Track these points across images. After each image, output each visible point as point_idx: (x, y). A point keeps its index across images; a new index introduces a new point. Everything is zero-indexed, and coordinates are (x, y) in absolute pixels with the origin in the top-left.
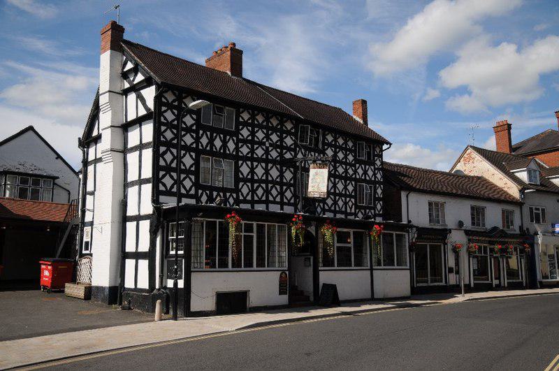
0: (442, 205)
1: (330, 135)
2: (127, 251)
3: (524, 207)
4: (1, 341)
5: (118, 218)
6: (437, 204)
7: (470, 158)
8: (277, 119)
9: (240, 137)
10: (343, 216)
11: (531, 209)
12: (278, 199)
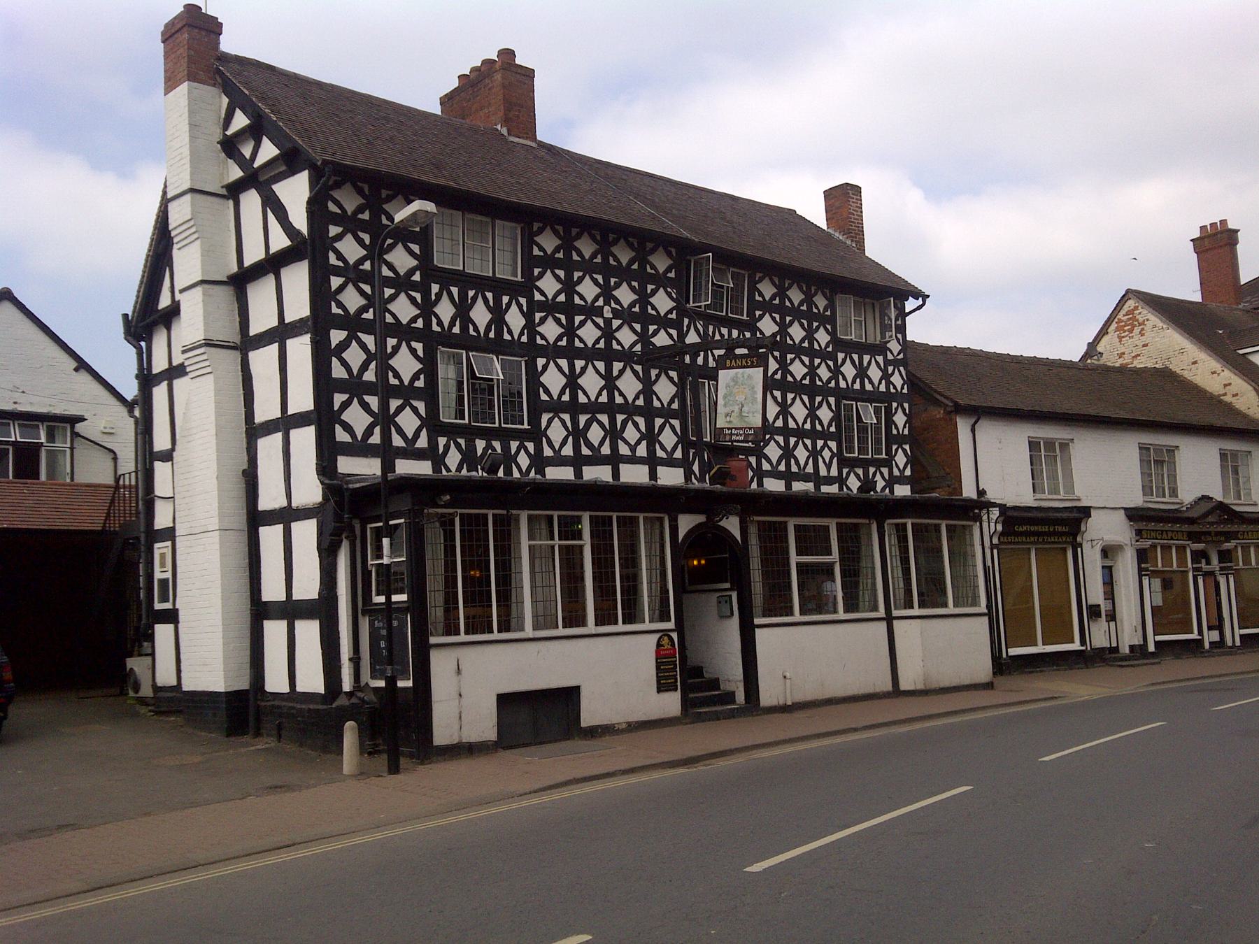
0: (1065, 446)
1: (548, 231)
6: (1050, 444)
9: (538, 297)
10: (810, 486)
12: (642, 451)
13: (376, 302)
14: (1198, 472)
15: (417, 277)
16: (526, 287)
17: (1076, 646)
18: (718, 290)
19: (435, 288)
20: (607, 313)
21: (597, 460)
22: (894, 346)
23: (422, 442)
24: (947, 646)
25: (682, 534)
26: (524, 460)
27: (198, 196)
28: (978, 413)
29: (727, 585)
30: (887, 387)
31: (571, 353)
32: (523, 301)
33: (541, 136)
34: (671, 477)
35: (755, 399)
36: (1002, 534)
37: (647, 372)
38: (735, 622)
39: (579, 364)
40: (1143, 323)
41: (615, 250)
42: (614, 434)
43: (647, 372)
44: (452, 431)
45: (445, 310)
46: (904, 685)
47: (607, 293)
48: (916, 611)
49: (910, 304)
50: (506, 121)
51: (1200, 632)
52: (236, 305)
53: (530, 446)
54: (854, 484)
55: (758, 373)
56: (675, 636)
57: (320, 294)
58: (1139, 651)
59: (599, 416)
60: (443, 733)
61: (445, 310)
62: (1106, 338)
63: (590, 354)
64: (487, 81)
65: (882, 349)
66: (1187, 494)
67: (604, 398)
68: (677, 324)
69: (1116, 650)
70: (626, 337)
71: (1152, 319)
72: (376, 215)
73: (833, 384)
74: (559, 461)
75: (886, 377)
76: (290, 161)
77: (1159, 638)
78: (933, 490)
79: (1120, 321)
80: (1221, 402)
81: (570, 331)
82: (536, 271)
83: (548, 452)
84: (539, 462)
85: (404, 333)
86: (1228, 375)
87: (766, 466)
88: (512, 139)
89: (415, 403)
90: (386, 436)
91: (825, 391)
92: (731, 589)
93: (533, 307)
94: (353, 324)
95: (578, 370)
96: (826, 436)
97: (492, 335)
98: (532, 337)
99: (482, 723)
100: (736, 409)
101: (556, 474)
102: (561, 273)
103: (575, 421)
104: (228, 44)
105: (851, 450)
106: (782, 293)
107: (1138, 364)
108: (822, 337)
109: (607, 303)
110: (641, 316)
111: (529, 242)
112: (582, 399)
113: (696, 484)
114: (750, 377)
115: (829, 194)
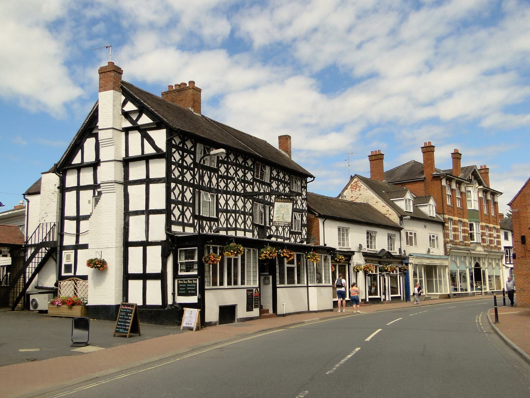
0: (347, 230)
1: (189, 140)
2: (129, 272)
3: (402, 232)
4: (1, 366)
5: (121, 244)
6: (343, 228)
7: (356, 186)
8: (180, 137)
9: (220, 174)
10: (282, 240)
11: (407, 233)
12: (242, 227)
14: (381, 242)
16: (216, 171)
22: (304, 193)
27: (115, 131)
28: (326, 217)
29: (267, 273)
32: (216, 174)
34: (249, 235)
35: (288, 213)
40: (360, 187)
49: (309, 179)
50: (193, 107)
51: (380, 295)
52: (123, 169)
57: (169, 171)
58: (364, 301)
64: (185, 91)
65: (301, 195)
66: (378, 249)
76: (158, 125)
79: (352, 185)
80: (385, 217)
86: (387, 208)
92: (270, 275)
94: (176, 181)
100: (281, 215)
107: (357, 201)
108: (249, 176)
110: (244, 181)
113: (254, 238)
114: (287, 206)
115: (280, 138)
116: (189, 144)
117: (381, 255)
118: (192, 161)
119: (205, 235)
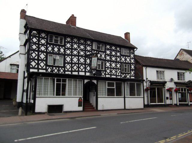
0: (163, 72)
6: (161, 72)
9: (66, 47)
10: (109, 76)
12: (84, 70)
13: (39, 48)
15: (45, 44)
17: (164, 103)
18: (125, 52)
19: (48, 46)
20: (79, 49)
21: (75, 71)
22: (132, 56)
23: (44, 67)
24: (136, 102)
25: (85, 83)
26: (62, 71)
28: (147, 66)
29: (94, 91)
30: (130, 62)
31: (111, 61)
32: (64, 48)
33: (77, 26)
35: (96, 61)
36: (150, 85)
37: (85, 59)
38: (95, 96)
39: (112, 63)
41: (81, 41)
42: (79, 67)
43: (85, 59)
44: (50, 66)
45: (50, 49)
46: (126, 108)
47: (79, 47)
48: (115, 96)
49: (135, 49)
51: (188, 102)
53: (63, 69)
54: (49, 70)
55: (96, 58)
56: (82, 98)
58: (176, 105)
59: (76, 65)
60: (37, 110)
61: (50, 49)
62: (178, 56)
63: (75, 56)
67: (77, 62)
68: (91, 51)
69: (172, 104)
70: (82, 53)
71: (185, 53)
72: (85, 43)
73: (120, 61)
74: (68, 71)
75: (130, 60)
77: (180, 103)
78: (140, 78)
81: (72, 52)
82: (66, 43)
83: (66, 70)
84: (64, 71)
85: (42, 52)
87: (107, 73)
88: (72, 26)
89: (44, 62)
90: (38, 66)
91: (119, 62)
93: (106, 55)
95: (73, 58)
96: (118, 69)
97: (58, 52)
98: (65, 53)
99: (44, 109)
101: (107, 76)
102: (71, 44)
103: (72, 65)
104: (27, 14)
105: (123, 71)
106: (116, 48)
108: (118, 54)
109: (79, 48)
111: (105, 47)
112: (73, 62)
115: (125, 34)
116: (118, 49)
117: (187, 83)
118: (75, 48)
119: (60, 74)
